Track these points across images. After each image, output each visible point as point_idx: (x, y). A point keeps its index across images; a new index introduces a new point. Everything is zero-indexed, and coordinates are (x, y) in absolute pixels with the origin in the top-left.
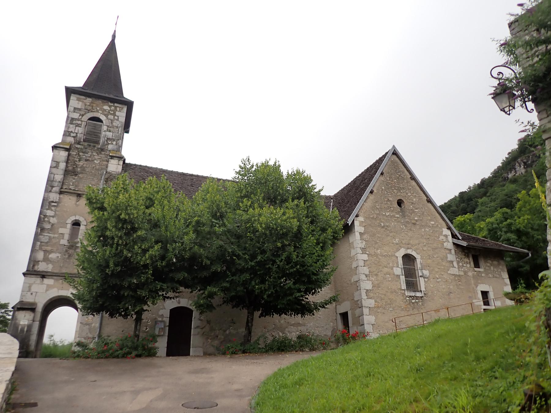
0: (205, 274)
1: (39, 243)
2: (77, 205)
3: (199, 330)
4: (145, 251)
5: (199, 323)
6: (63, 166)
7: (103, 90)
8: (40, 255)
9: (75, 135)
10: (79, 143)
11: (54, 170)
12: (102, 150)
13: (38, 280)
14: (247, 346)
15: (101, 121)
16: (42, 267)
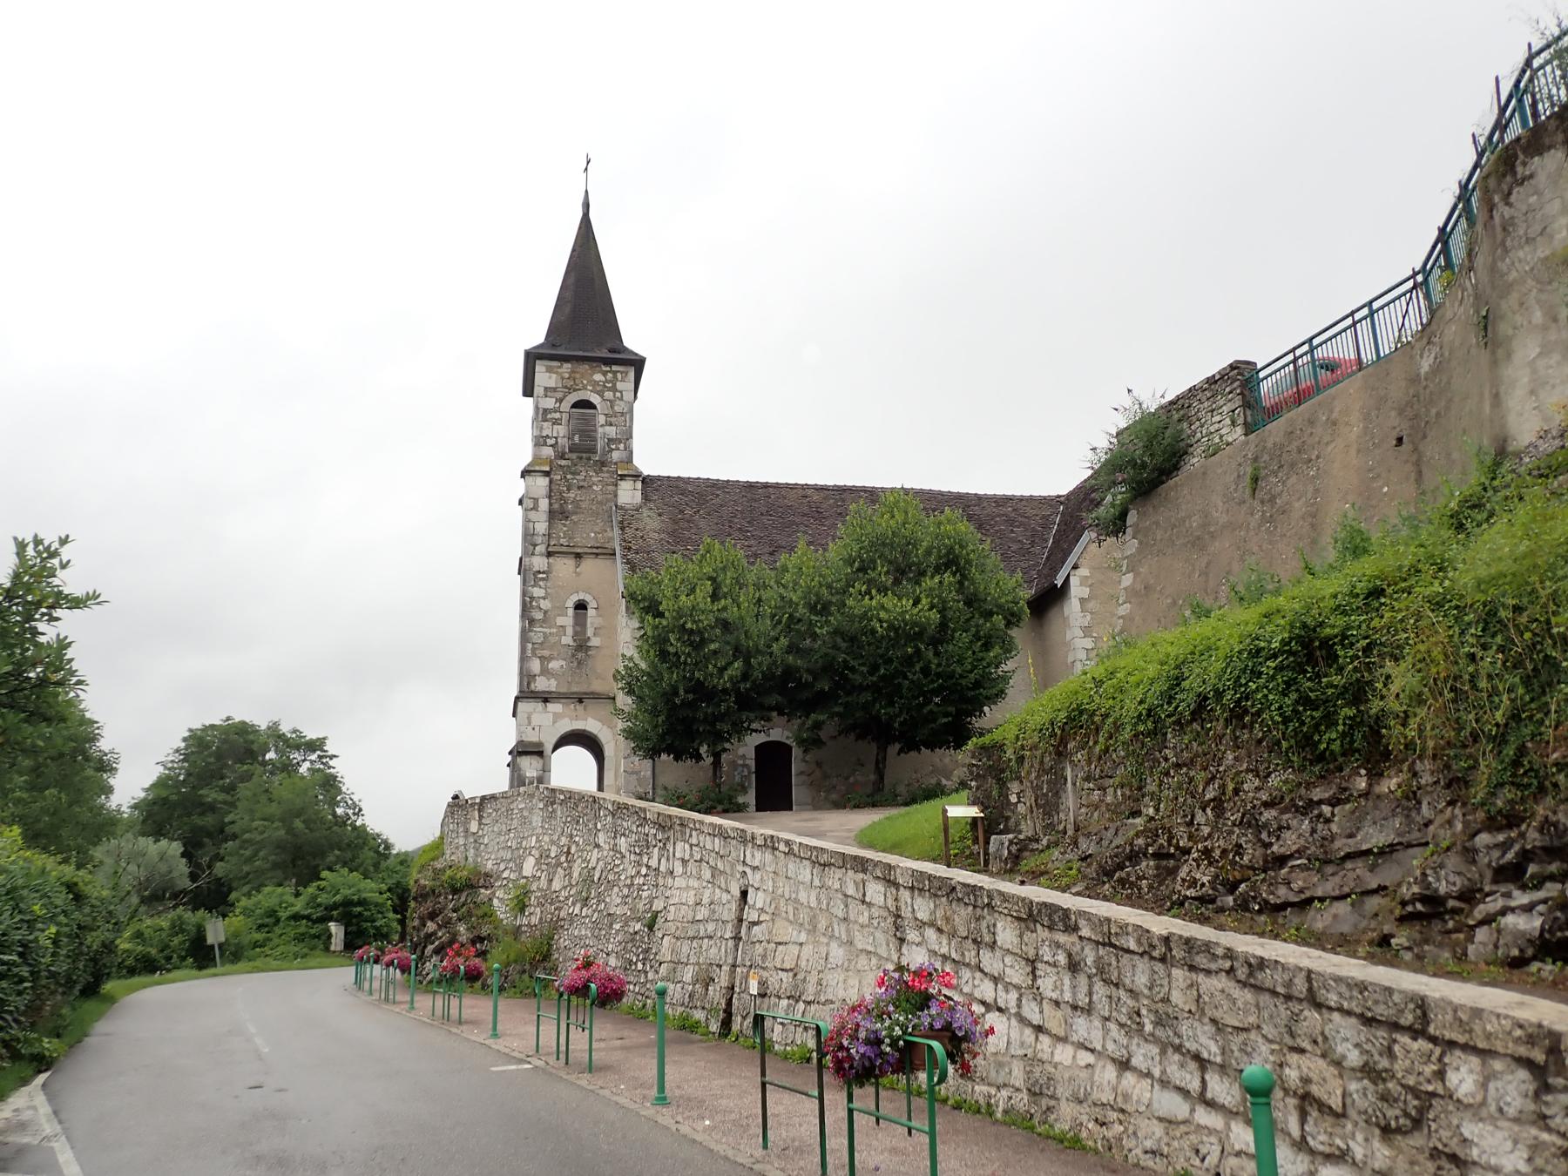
0: (805, 695)
1: (530, 646)
2: (578, 574)
3: (804, 778)
4: (722, 670)
5: (803, 766)
6: (544, 504)
7: (584, 334)
8: (535, 666)
9: (553, 441)
10: (562, 457)
11: (533, 515)
12: (603, 464)
13: (540, 705)
14: (877, 797)
15: (592, 406)
16: (541, 684)
